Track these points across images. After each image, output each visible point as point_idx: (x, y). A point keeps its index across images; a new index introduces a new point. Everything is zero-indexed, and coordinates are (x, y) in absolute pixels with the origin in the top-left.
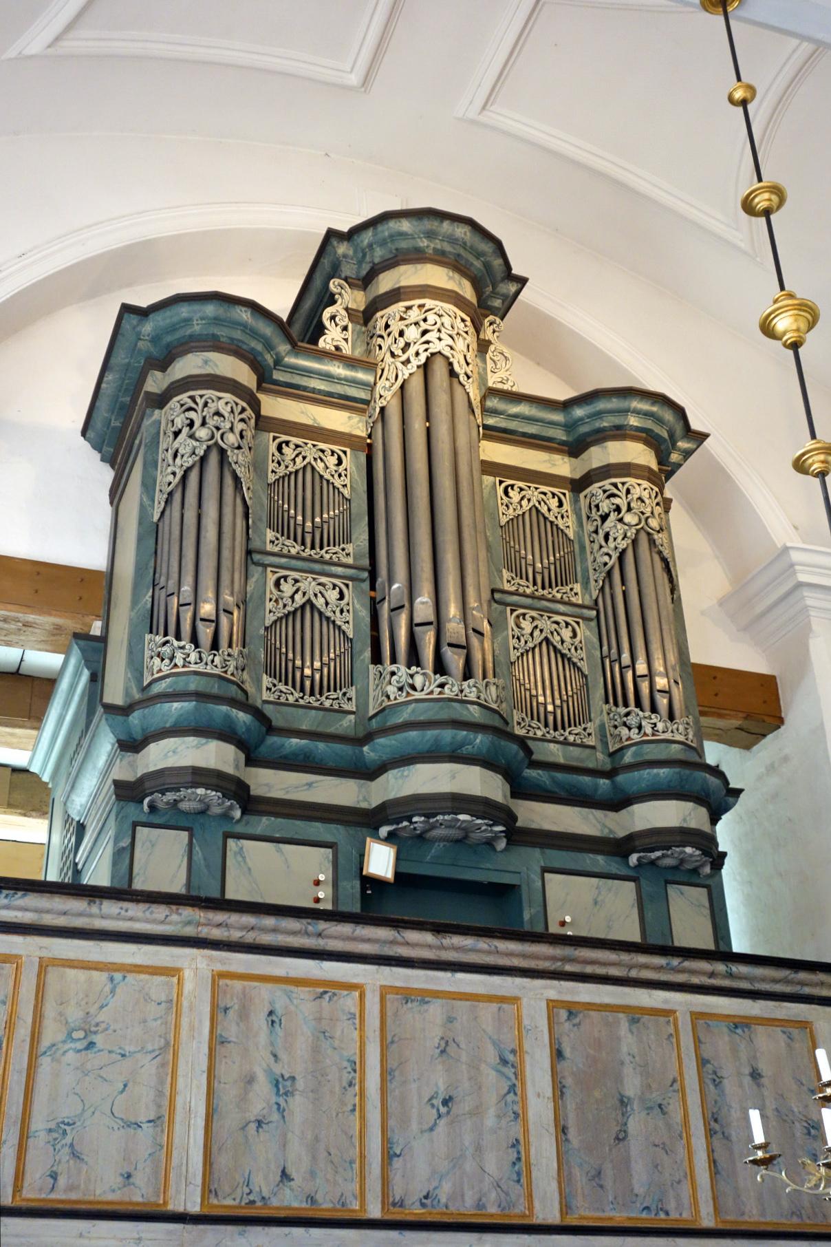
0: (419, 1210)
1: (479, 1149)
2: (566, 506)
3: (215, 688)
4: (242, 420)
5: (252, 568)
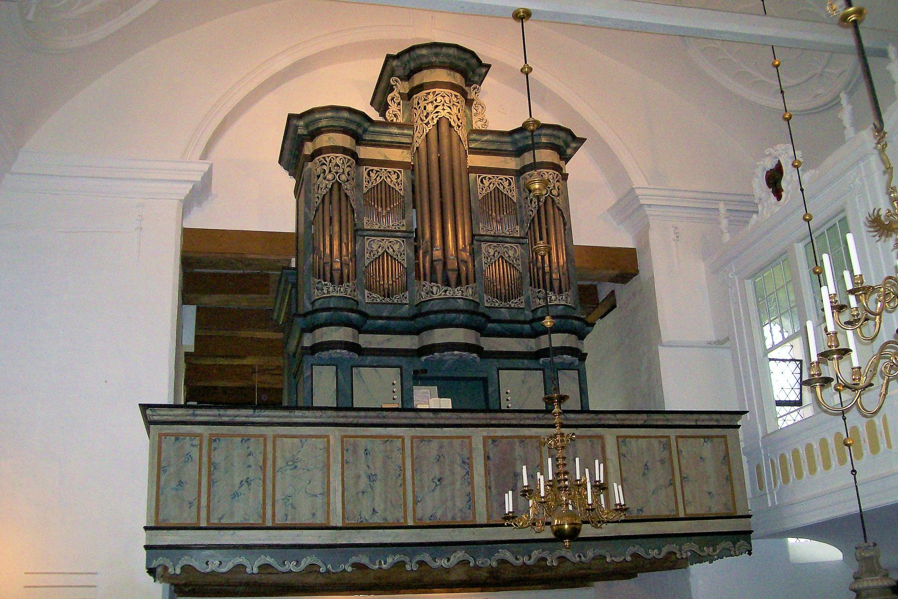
0: (428, 521)
1: (453, 496)
2: (513, 185)
3: (341, 304)
4: (349, 166)
5: (358, 238)
